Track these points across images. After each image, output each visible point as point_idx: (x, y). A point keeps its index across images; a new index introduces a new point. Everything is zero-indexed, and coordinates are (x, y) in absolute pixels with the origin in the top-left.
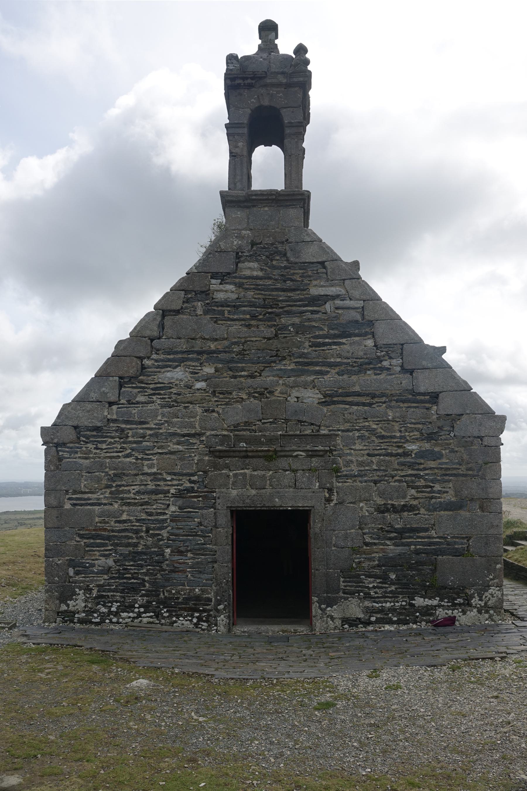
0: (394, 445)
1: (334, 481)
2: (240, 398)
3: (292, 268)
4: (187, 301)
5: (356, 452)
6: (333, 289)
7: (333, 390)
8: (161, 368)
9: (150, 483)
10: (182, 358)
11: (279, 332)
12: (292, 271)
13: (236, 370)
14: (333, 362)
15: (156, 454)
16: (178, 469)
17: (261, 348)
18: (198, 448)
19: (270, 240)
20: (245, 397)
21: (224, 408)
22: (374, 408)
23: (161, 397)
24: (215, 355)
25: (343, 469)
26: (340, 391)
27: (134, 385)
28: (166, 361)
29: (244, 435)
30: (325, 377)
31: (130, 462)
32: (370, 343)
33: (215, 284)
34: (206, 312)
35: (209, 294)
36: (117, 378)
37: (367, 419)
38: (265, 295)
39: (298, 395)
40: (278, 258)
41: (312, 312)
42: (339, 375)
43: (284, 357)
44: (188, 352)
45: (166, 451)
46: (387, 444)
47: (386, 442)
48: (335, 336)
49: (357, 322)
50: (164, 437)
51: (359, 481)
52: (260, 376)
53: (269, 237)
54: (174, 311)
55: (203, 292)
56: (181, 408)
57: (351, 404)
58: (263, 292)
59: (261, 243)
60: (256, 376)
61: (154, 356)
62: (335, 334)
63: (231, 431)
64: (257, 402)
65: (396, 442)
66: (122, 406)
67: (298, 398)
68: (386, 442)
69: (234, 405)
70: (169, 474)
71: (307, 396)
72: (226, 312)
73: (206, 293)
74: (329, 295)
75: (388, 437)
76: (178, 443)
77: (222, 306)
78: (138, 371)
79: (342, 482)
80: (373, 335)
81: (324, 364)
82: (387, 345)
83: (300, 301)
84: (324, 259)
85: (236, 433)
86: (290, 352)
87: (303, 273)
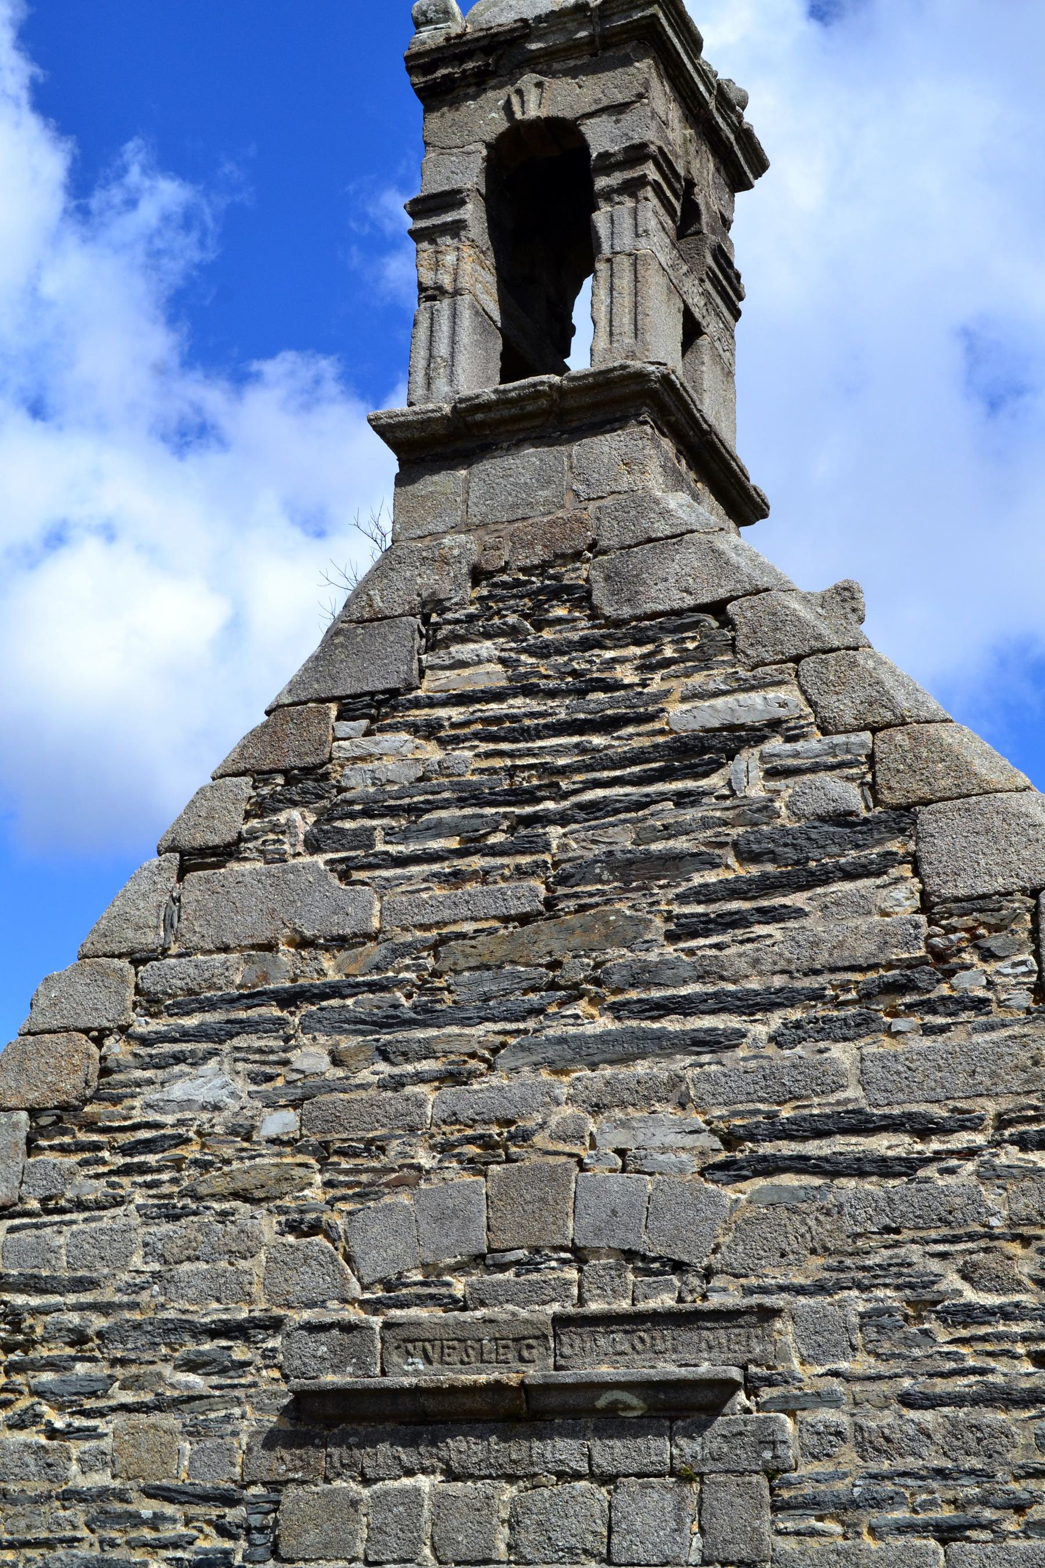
0: (1020, 1349)
1: (766, 1528)
2: (411, 1166)
3: (608, 643)
4: (260, 808)
5: (857, 1387)
6: (755, 698)
7: (758, 1112)
8: (157, 1067)
9: (84, 1533)
10: (228, 1022)
11: (561, 891)
12: (609, 654)
13: (404, 1054)
14: (756, 993)
15: (113, 1409)
16: (180, 1474)
17: (492, 962)
18: (254, 1385)
19: (538, 555)
20: (425, 1159)
21: (350, 1213)
22: (927, 1180)
23: (149, 1178)
24: (334, 1002)
25: (803, 1471)
26: (786, 1113)
27: (67, 1139)
28: (175, 1041)
29: (417, 1324)
30: (727, 1057)
31: (27, 1446)
32: (902, 897)
33: (349, 737)
34: (313, 846)
35: (326, 777)
36: (24, 1115)
37: (897, 1231)
38: (511, 755)
39: (620, 1138)
40: (561, 612)
41: (682, 799)
42: (780, 1045)
43: (576, 985)
44: (253, 998)
45: (148, 1397)
46: (989, 1347)
47: (984, 1339)
48: (766, 886)
49: (842, 818)
50: (144, 1340)
51: (872, 1530)
52: (491, 1067)
53: (531, 545)
54: (213, 850)
55: (308, 771)
56: (208, 1217)
57: (829, 1169)
58: (505, 746)
59: (503, 570)
60: (473, 1074)
61: (143, 1026)
62: (765, 876)
63: (373, 1307)
64: (468, 1178)
65: (1026, 1338)
66: (26, 1220)
67: (621, 1152)
68: (984, 1339)
69: (387, 1200)
70: (152, 1493)
71: (656, 1142)
72: (379, 835)
73: (308, 780)
74: (742, 727)
75: (990, 1313)
76: (191, 1365)
77: (367, 813)
78: (86, 1082)
79: (798, 1533)
80: (915, 861)
81: (721, 1004)
82: (977, 902)
83: (633, 762)
84: (722, 593)
85: (396, 1313)
86: (598, 965)
87: (643, 657)
